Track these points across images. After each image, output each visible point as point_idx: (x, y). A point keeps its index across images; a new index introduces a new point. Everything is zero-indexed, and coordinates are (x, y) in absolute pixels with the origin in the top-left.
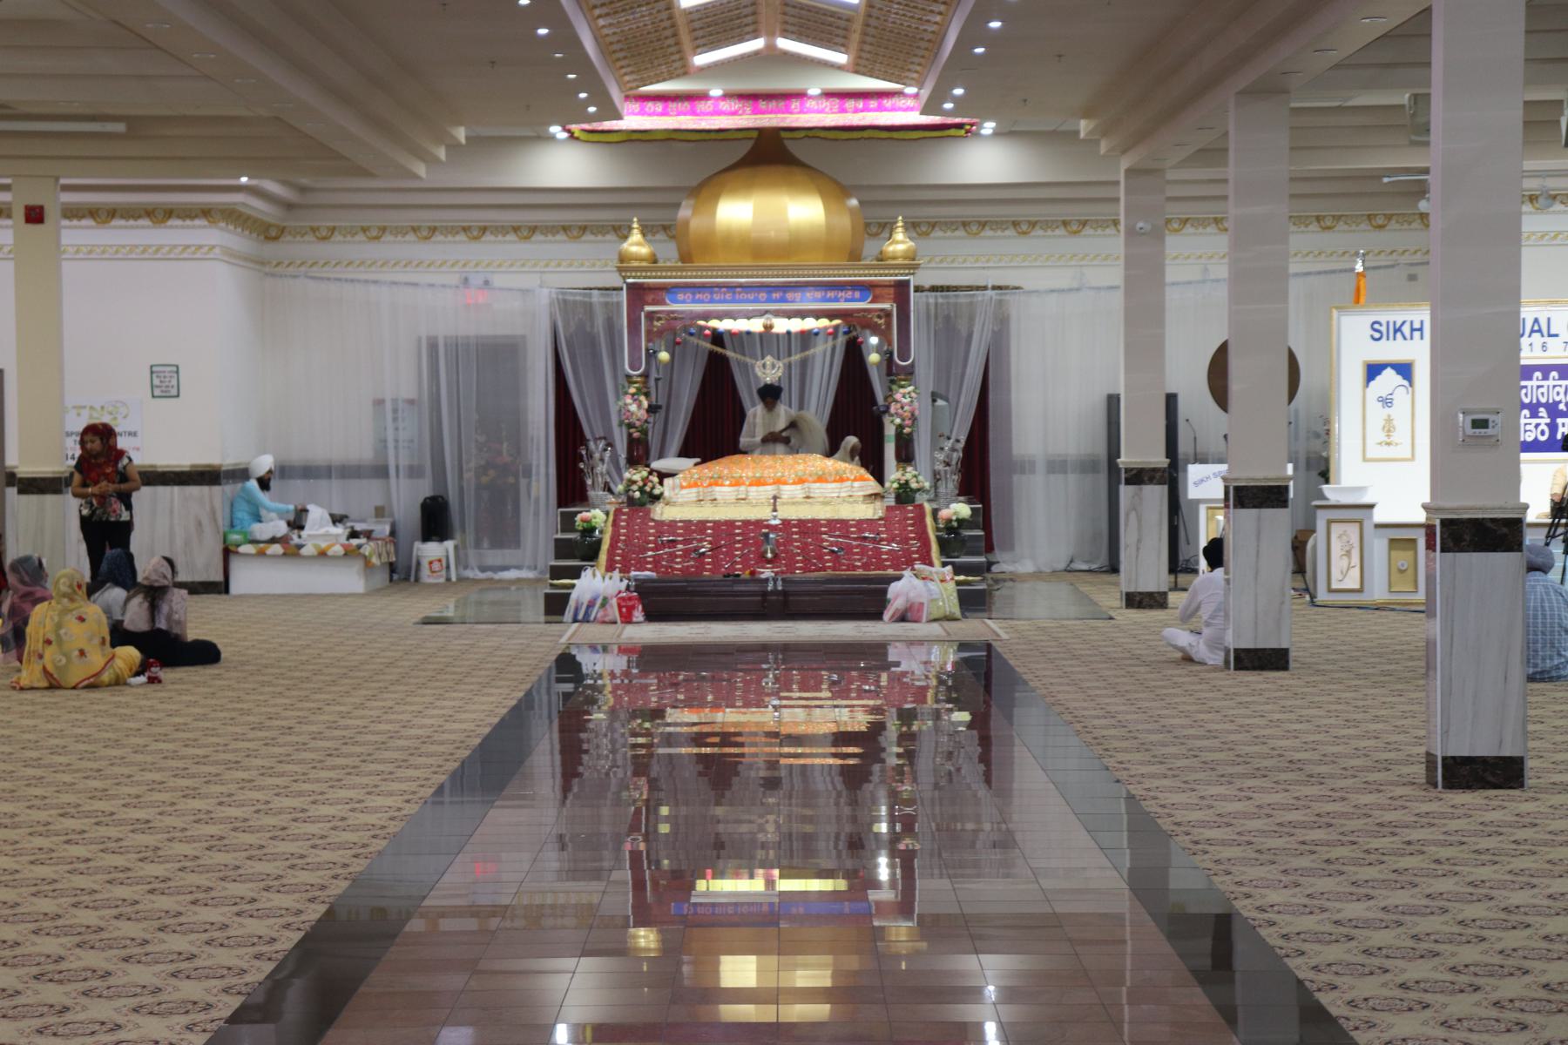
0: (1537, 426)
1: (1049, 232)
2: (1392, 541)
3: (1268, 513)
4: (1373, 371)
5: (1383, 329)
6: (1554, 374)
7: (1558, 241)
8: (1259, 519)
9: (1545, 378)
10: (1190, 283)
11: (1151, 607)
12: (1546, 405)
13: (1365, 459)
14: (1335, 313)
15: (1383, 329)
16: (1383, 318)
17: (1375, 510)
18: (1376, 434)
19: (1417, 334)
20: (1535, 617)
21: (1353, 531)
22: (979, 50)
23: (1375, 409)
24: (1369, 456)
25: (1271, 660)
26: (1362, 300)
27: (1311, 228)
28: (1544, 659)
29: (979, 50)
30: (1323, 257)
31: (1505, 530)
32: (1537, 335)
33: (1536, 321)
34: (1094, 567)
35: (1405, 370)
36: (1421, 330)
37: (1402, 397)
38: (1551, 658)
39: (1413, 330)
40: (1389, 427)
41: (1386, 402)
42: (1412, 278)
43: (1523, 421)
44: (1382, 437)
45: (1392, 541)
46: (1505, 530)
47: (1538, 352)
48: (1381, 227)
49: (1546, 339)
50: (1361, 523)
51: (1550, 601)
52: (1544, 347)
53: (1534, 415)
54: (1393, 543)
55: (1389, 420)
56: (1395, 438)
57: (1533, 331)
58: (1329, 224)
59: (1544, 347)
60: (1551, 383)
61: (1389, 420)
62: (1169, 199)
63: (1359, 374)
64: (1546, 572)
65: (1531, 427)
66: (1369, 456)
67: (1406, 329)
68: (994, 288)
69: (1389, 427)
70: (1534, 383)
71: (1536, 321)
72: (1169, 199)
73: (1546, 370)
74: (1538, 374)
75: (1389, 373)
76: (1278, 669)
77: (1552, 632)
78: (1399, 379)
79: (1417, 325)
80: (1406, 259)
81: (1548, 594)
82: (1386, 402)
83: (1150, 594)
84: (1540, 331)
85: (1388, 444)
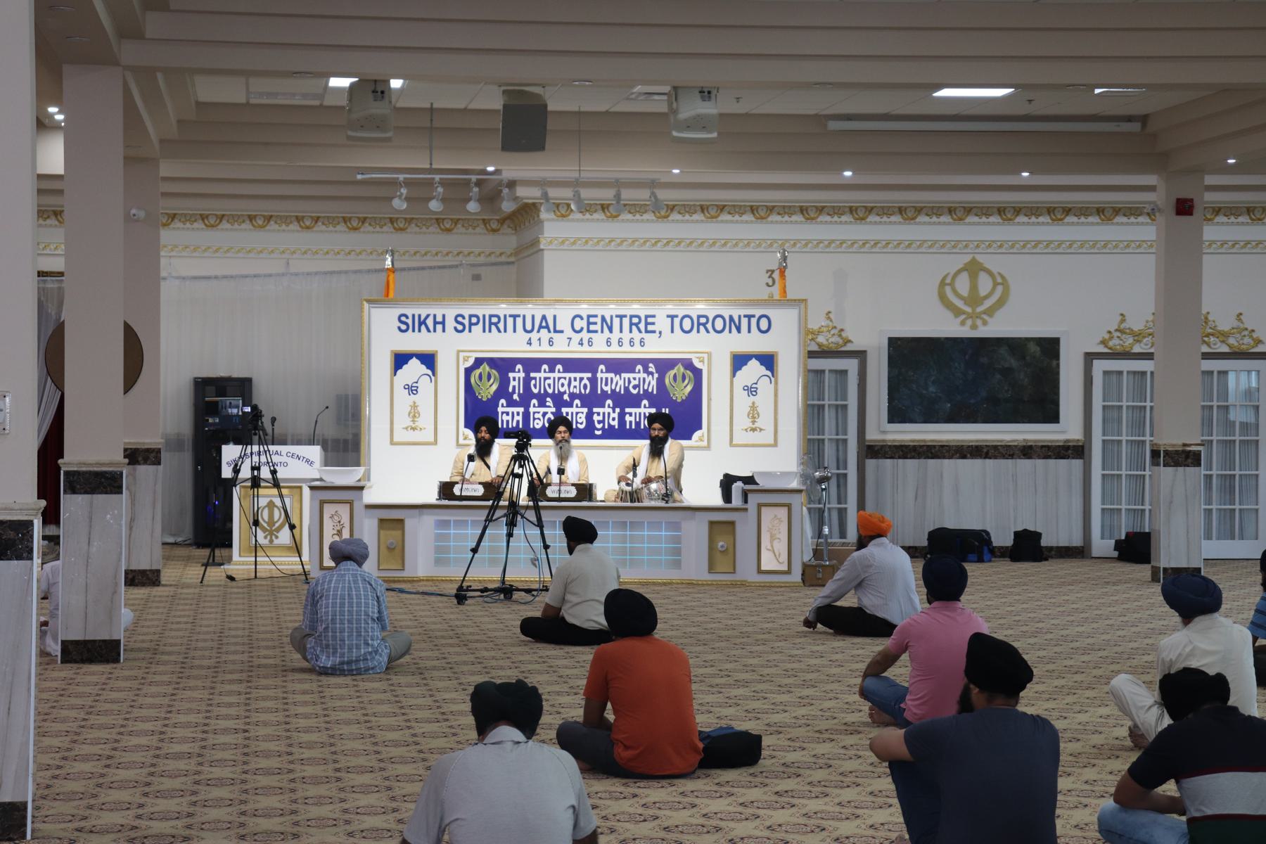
0: (545, 414)
1: (236, 226)
2: (382, 521)
3: (100, 499)
4: (400, 360)
5: (410, 321)
6: (559, 367)
7: (623, 247)
8: (91, 503)
9: (552, 370)
10: (270, 275)
11: (143, 584)
12: (553, 396)
13: (392, 443)
14: (366, 305)
15: (410, 321)
16: (409, 312)
17: (365, 491)
18: (402, 420)
19: (439, 327)
20: (342, 605)
21: (344, 511)
22: (1231, 161)
23: (401, 395)
24: (396, 439)
25: (98, 652)
26: (391, 295)
27: (385, 229)
28: (350, 649)
29: (1231, 161)
30: (353, 256)
31: (11, 534)
32: (544, 331)
33: (544, 317)
34: (179, 539)
35: (768, 361)
36: (443, 323)
37: (425, 386)
38: (358, 647)
39: (435, 323)
40: (414, 413)
41: (751, 390)
42: (477, 277)
43: (500, 409)
44: (408, 422)
45: (382, 521)
46: (11, 534)
47: (545, 346)
48: (449, 230)
49: (552, 335)
50: (351, 503)
51: (357, 589)
52: (551, 342)
53: (542, 404)
54: (383, 522)
55: (414, 406)
56: (419, 423)
57: (541, 327)
58: (401, 225)
59: (551, 342)
60: (556, 375)
61: (414, 406)
62: (164, 194)
63: (388, 362)
64: (360, 564)
65: (539, 416)
66: (396, 439)
67: (430, 322)
68: (178, 278)
69: (414, 413)
70: (542, 375)
71: (544, 317)
72: (164, 194)
73: (552, 363)
74: (545, 367)
75: (414, 362)
76: (107, 661)
77: (358, 621)
78: (763, 370)
79: (439, 319)
80: (471, 259)
81: (356, 582)
82: (412, 389)
83: (143, 572)
84: (547, 327)
85: (414, 429)
